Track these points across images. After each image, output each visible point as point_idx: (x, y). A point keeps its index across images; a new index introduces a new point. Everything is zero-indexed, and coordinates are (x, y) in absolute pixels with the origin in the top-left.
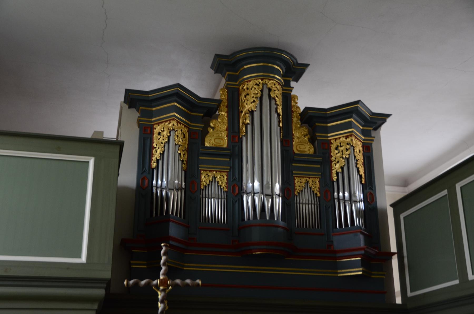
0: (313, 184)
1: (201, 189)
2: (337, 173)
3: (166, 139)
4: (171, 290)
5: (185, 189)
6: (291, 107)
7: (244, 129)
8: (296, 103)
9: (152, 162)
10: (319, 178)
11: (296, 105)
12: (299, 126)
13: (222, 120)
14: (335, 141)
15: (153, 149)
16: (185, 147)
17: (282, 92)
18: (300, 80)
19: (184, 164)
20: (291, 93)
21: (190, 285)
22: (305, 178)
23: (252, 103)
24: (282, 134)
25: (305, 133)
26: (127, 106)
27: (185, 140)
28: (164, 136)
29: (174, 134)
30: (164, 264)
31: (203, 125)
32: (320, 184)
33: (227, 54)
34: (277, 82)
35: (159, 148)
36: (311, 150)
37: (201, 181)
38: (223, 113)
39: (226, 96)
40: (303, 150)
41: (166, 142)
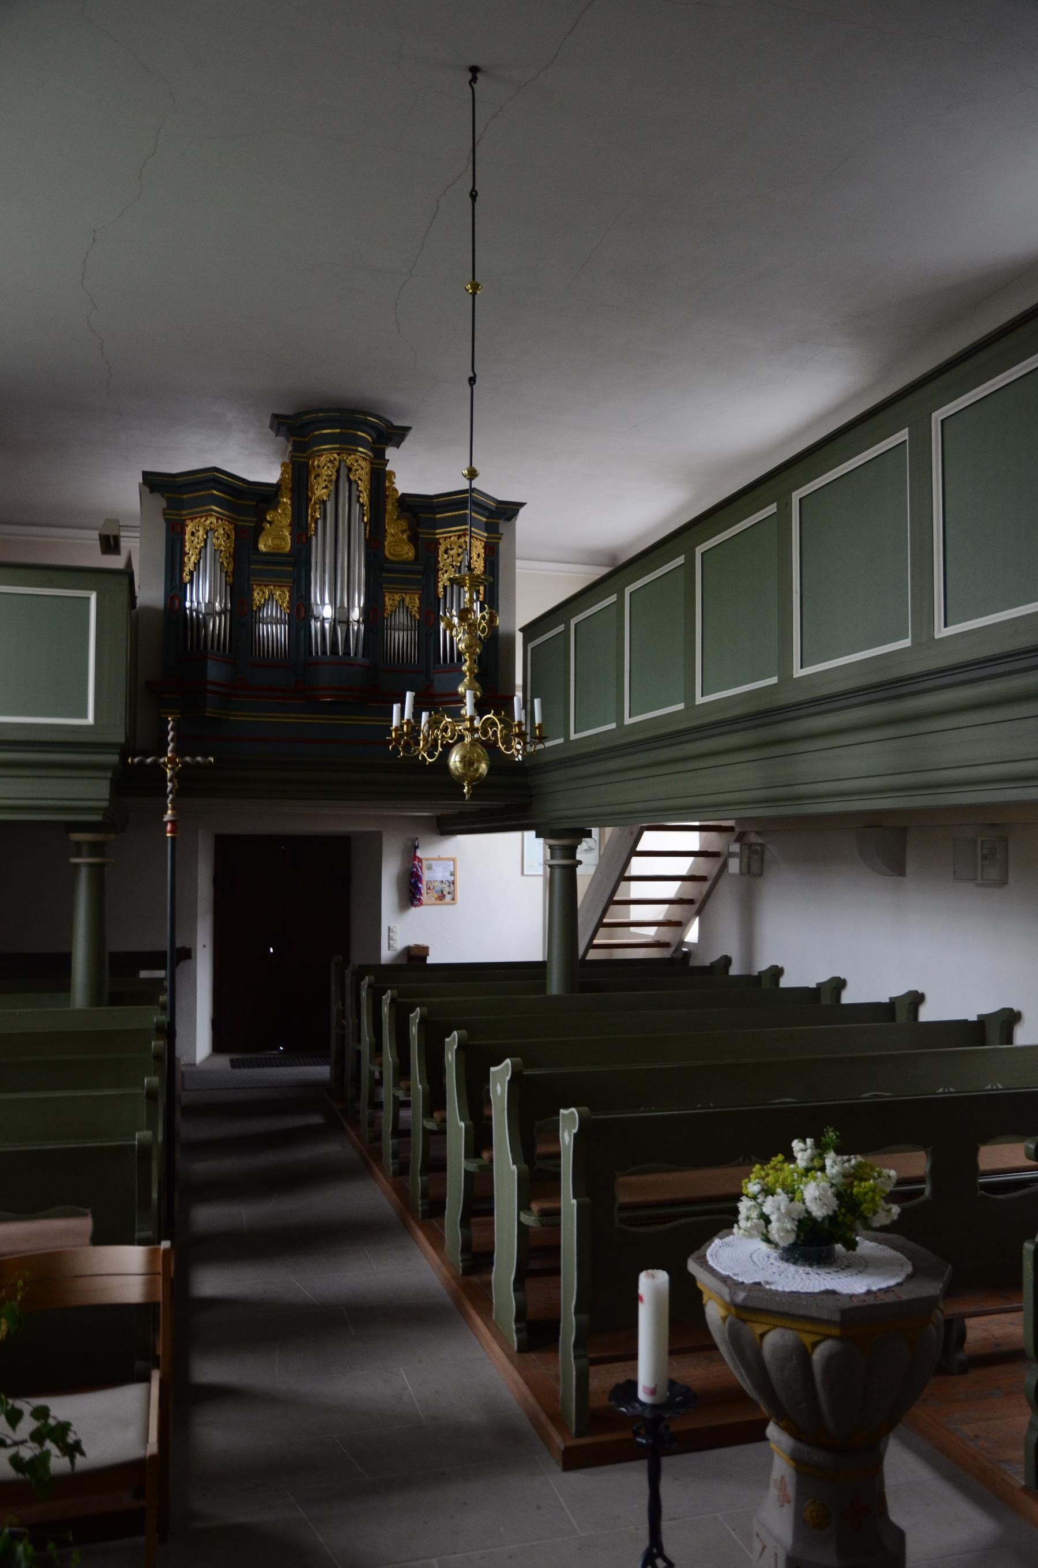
0: (411, 602)
1: (253, 611)
2: (445, 588)
3: (201, 543)
4: (181, 768)
5: (231, 611)
6: (385, 489)
7: (313, 525)
8: (393, 483)
9: (184, 574)
10: (420, 594)
11: (393, 486)
12: (395, 517)
13: (283, 510)
14: (445, 540)
15: (185, 556)
16: (230, 553)
17: (371, 468)
18: (403, 445)
19: (229, 576)
20: (385, 469)
21: (202, 763)
22: (400, 594)
23: (323, 488)
24: (367, 532)
25: (404, 528)
26: (147, 489)
27: (229, 543)
28: (198, 538)
29: (213, 536)
30: (172, 740)
31: (255, 519)
32: (420, 602)
33: (291, 413)
34: (360, 456)
35: (192, 555)
36: (410, 554)
37: (253, 600)
38: (285, 500)
39: (290, 474)
40: (398, 553)
41: (202, 547)
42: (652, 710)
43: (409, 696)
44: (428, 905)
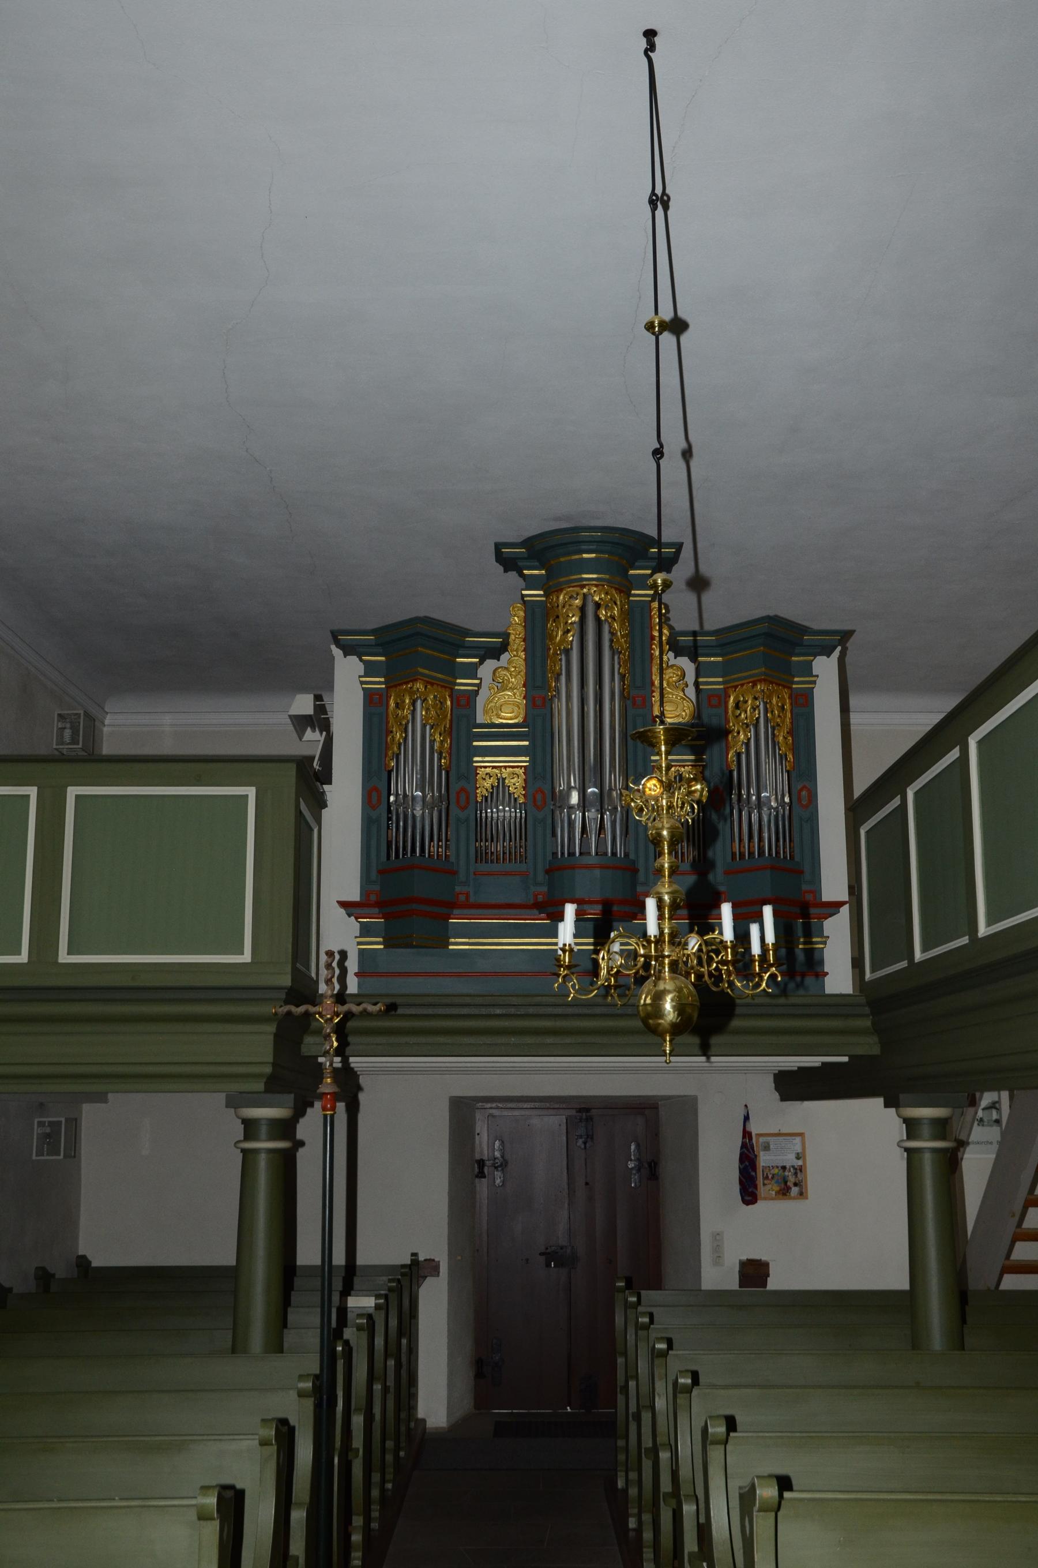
1: (477, 802)
19: (445, 758)
42: (243, 935)
43: (768, 911)
44: (765, 1199)
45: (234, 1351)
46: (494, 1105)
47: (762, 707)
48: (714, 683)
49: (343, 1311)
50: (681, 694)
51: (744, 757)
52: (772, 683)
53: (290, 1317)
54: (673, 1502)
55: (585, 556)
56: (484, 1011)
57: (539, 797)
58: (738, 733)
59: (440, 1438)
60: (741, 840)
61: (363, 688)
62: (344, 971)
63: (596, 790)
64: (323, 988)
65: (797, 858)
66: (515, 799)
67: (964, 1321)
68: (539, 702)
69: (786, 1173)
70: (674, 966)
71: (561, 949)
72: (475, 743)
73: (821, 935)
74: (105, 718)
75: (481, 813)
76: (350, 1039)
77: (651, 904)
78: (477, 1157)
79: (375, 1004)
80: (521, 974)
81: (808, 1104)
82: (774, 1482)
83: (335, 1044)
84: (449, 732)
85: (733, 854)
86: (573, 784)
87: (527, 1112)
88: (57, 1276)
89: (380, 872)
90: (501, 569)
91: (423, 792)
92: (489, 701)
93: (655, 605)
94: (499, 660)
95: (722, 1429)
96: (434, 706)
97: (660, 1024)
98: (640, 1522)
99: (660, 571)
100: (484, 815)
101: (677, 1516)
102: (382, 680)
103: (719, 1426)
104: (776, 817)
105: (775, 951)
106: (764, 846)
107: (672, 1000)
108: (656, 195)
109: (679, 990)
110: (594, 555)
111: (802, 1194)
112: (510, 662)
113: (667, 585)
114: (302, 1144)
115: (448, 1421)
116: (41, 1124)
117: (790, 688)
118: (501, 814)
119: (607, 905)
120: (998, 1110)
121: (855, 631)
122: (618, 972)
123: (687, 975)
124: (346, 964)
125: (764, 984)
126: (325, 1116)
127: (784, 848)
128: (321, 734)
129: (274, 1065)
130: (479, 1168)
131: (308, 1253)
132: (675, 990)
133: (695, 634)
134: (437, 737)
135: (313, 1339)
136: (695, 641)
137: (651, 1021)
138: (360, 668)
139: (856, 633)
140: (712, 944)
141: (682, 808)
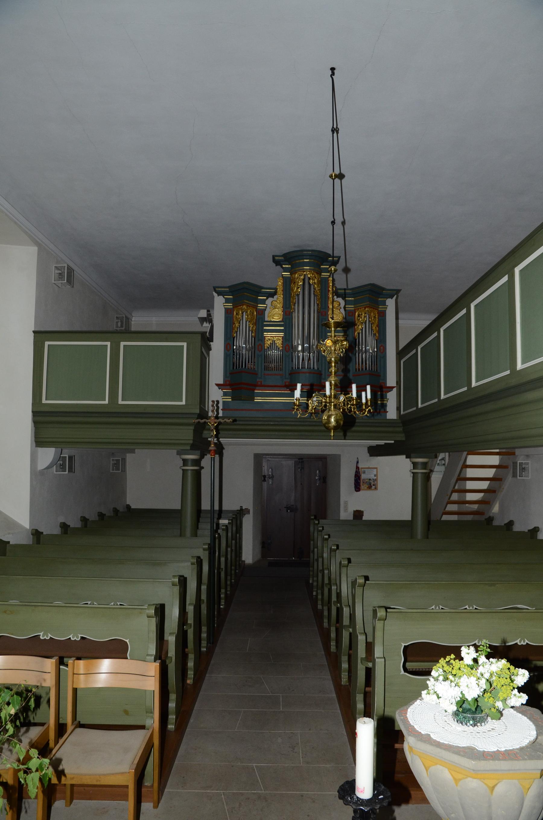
1: (265, 349)
19: (254, 333)
42: (105, 392)
43: (368, 387)
44: (363, 490)
45: (181, 536)
46: (269, 457)
47: (368, 316)
48: (350, 307)
49: (218, 524)
50: (339, 311)
51: (361, 334)
52: (371, 308)
53: (199, 526)
54: (329, 586)
55: (305, 260)
56: (266, 423)
57: (287, 347)
58: (359, 326)
59: (250, 567)
60: (359, 364)
61: (225, 308)
62: (218, 407)
63: (308, 345)
64: (210, 414)
65: (379, 371)
66: (279, 348)
67: (429, 529)
68: (288, 313)
69: (371, 481)
70: (335, 406)
71: (296, 399)
72: (265, 328)
73: (387, 399)
74: (132, 318)
75: (266, 353)
76: (220, 432)
77: (327, 384)
78: (263, 474)
79: (229, 419)
80: (281, 410)
81: (379, 458)
82: (363, 577)
83: (215, 433)
84: (255, 324)
85: (356, 369)
86: (299, 343)
87: (281, 459)
88: (120, 511)
89: (230, 374)
90: (275, 265)
91: (246, 345)
92: (270, 313)
93: (331, 279)
94: (273, 298)
95: (346, 562)
96: (250, 314)
97: (329, 426)
98: (317, 593)
99: (333, 265)
100: (267, 354)
101: (330, 590)
102: (231, 304)
103: (345, 561)
104: (372, 356)
105: (370, 401)
106: (367, 366)
107: (334, 418)
108: (334, 128)
109: (337, 415)
110: (308, 260)
111: (376, 489)
112: (277, 298)
113: (336, 270)
114: (203, 468)
115: (253, 559)
116: (113, 460)
117: (378, 310)
118: (274, 353)
119: (312, 385)
120: (445, 460)
121: (401, 290)
122: (315, 408)
123: (340, 409)
124: (219, 405)
125: (366, 413)
126: (212, 458)
127: (374, 367)
128: (209, 324)
129: (193, 440)
130: (264, 478)
131: (205, 505)
132: (335, 415)
133: (345, 289)
134: (251, 326)
135: (208, 533)
136: (345, 292)
137: (326, 425)
138: (224, 300)
139: (402, 291)
140: (348, 399)
141: (339, 350)
